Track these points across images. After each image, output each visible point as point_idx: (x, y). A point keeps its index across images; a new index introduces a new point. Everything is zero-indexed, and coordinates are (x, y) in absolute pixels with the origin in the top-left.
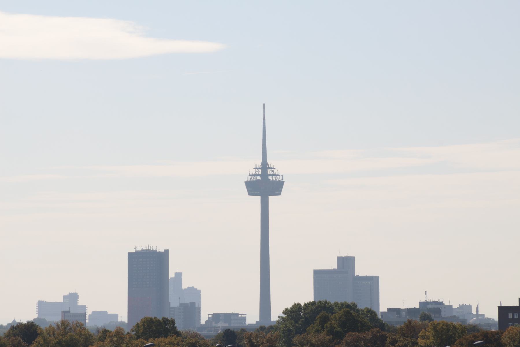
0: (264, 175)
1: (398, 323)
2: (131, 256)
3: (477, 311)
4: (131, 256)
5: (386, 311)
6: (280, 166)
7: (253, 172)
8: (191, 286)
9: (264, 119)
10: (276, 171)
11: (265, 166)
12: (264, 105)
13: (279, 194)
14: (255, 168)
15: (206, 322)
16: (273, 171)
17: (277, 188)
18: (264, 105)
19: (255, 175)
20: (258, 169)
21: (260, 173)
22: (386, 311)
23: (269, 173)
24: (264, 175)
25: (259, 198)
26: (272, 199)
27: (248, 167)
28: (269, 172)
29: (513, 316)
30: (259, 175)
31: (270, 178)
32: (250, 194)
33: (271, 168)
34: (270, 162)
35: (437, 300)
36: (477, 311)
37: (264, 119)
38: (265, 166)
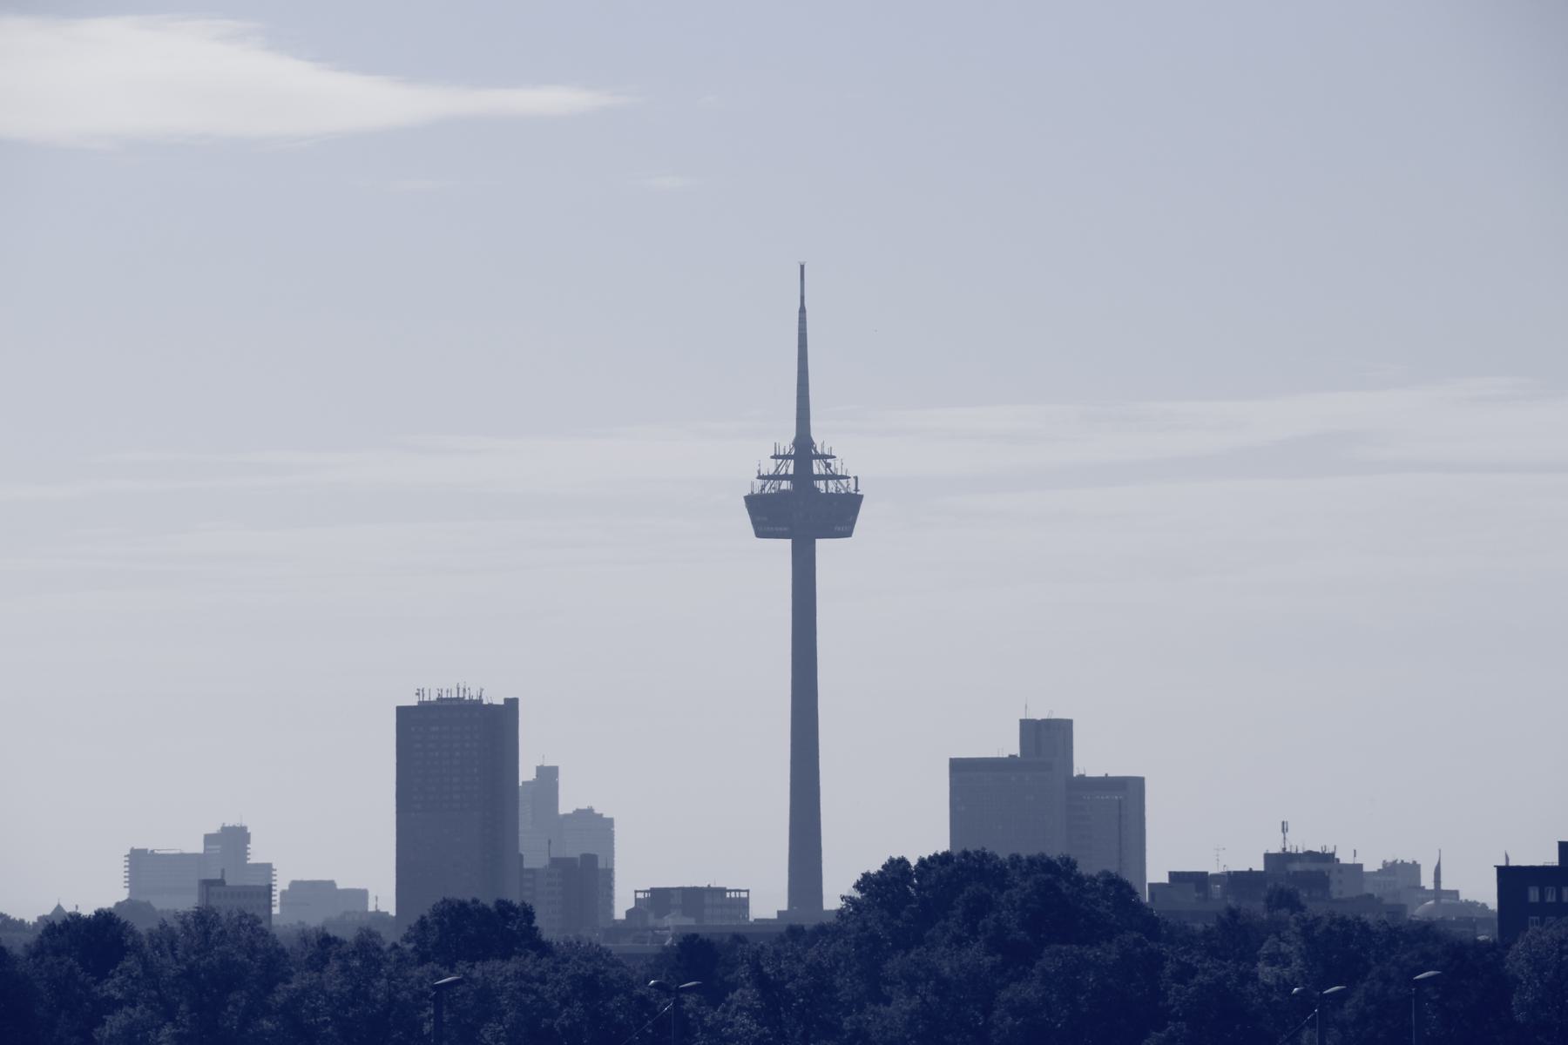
0: (803, 476)
3: (1437, 880)
6: (850, 451)
7: (769, 467)
9: (802, 310)
10: (836, 466)
11: (804, 449)
12: (802, 267)
14: (776, 457)
16: (828, 466)
17: (768, 513)
18: (802, 267)
21: (791, 471)
23: (816, 471)
24: (803, 476)
25: (786, 544)
27: (756, 454)
28: (818, 467)
30: (786, 477)
32: (760, 533)
33: (824, 457)
34: (820, 438)
35: (1318, 849)
36: (1437, 880)
37: (802, 310)
38: (804, 449)
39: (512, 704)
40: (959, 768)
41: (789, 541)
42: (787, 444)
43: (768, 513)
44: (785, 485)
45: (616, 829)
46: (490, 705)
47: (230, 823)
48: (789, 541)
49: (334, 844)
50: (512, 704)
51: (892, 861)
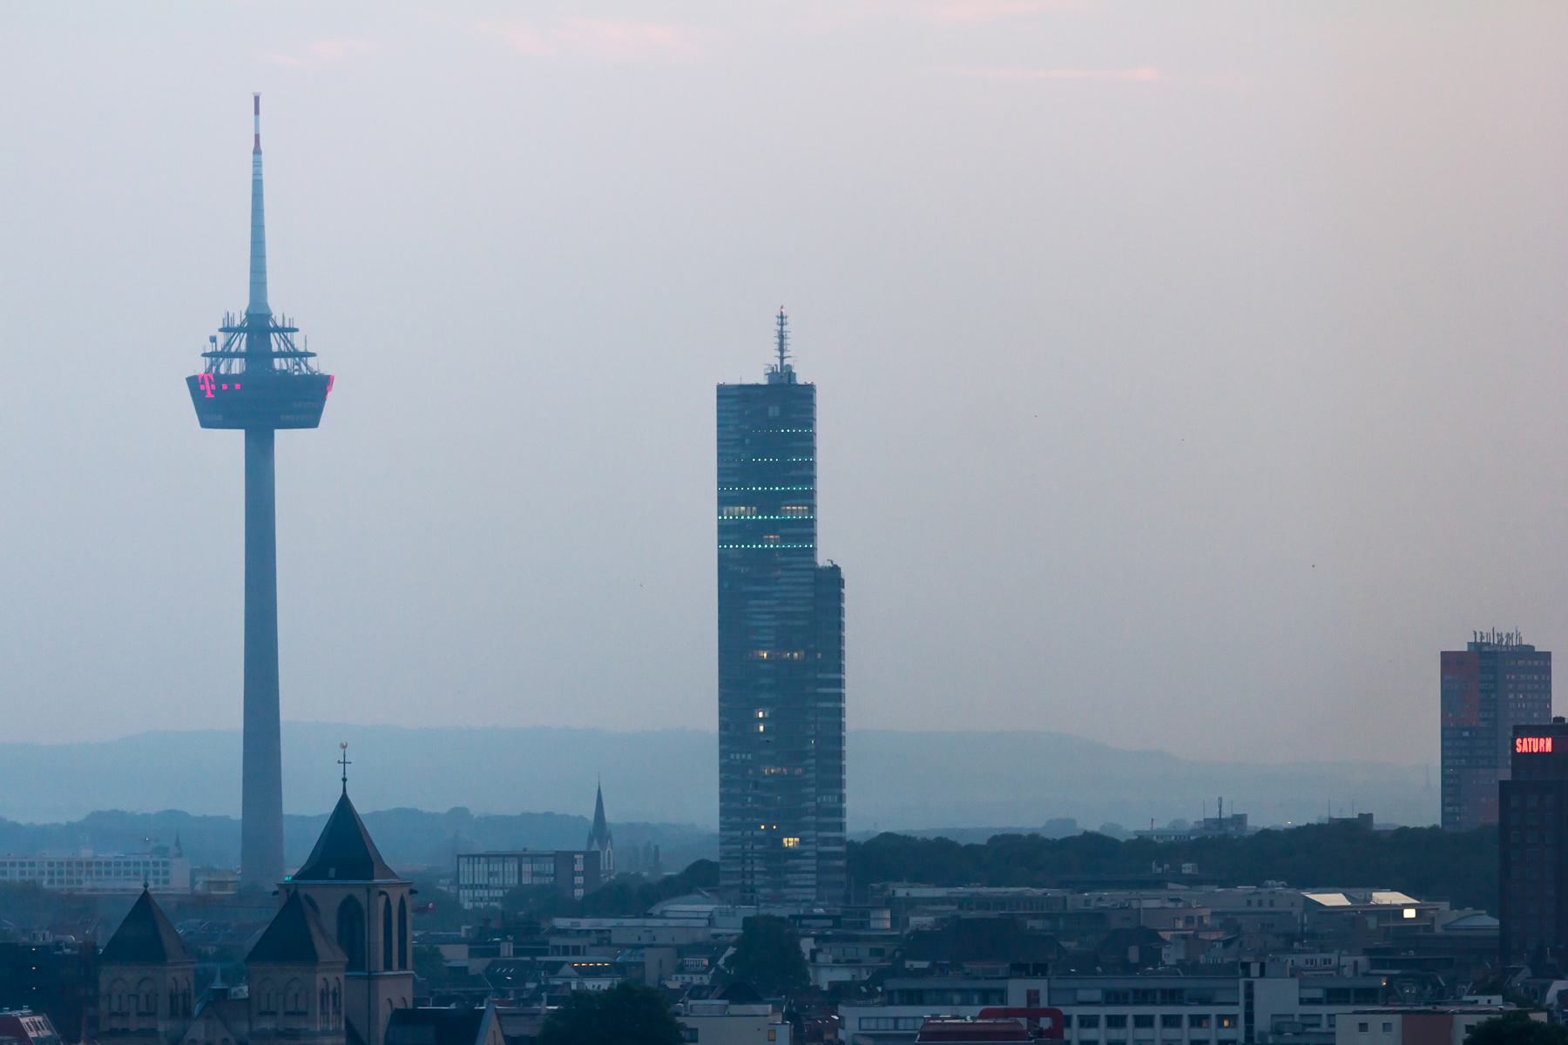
0: (258, 353)
1: (480, 893)
5: (822, 560)
6: (320, 334)
10: (299, 343)
11: (258, 325)
12: (257, 99)
13: (313, 423)
15: (1490, 914)
18: (257, 99)
19: (226, 354)
20: (239, 330)
21: (243, 348)
22: (822, 560)
23: (275, 348)
24: (258, 353)
27: (190, 340)
28: (276, 342)
29: (579, 887)
30: (238, 355)
31: (278, 363)
32: (205, 424)
34: (280, 308)
38: (258, 325)
40: (724, 393)
41: (242, 432)
42: (238, 307)
43: (218, 401)
44: (237, 366)
45: (729, 382)
46: (1266, 833)
48: (242, 432)
49: (512, 657)
51: (456, 810)
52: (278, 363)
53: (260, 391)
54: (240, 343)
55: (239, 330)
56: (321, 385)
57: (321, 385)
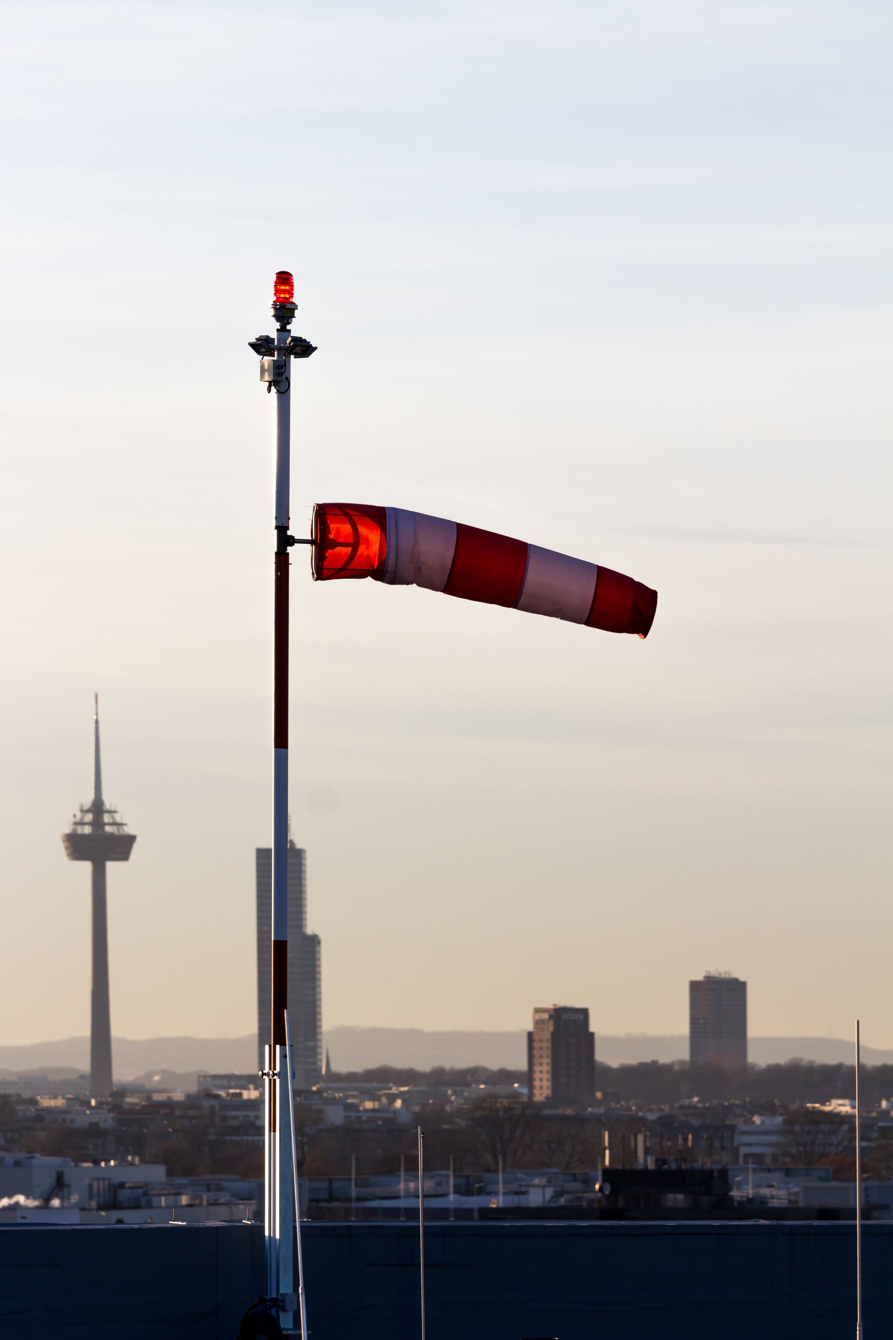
0: (98, 824)
2: (695, 986)
3: (287, 970)
4: (695, 986)
6: (128, 812)
8: (742, 979)
9: (97, 722)
10: (118, 818)
11: (98, 808)
12: (96, 696)
16: (113, 818)
18: (96, 696)
24: (98, 824)
26: (112, 867)
27: (66, 812)
28: (107, 818)
31: (690, 1144)
33: (110, 812)
34: (109, 801)
36: (287, 970)
37: (97, 722)
38: (98, 808)
39: (316, 348)
42: (88, 799)
44: (87, 830)
47: (735, 975)
50: (316, 348)
52: (108, 829)
53: (99, 843)
54: (89, 817)
55: (88, 811)
56: (130, 840)
57: (130, 840)
